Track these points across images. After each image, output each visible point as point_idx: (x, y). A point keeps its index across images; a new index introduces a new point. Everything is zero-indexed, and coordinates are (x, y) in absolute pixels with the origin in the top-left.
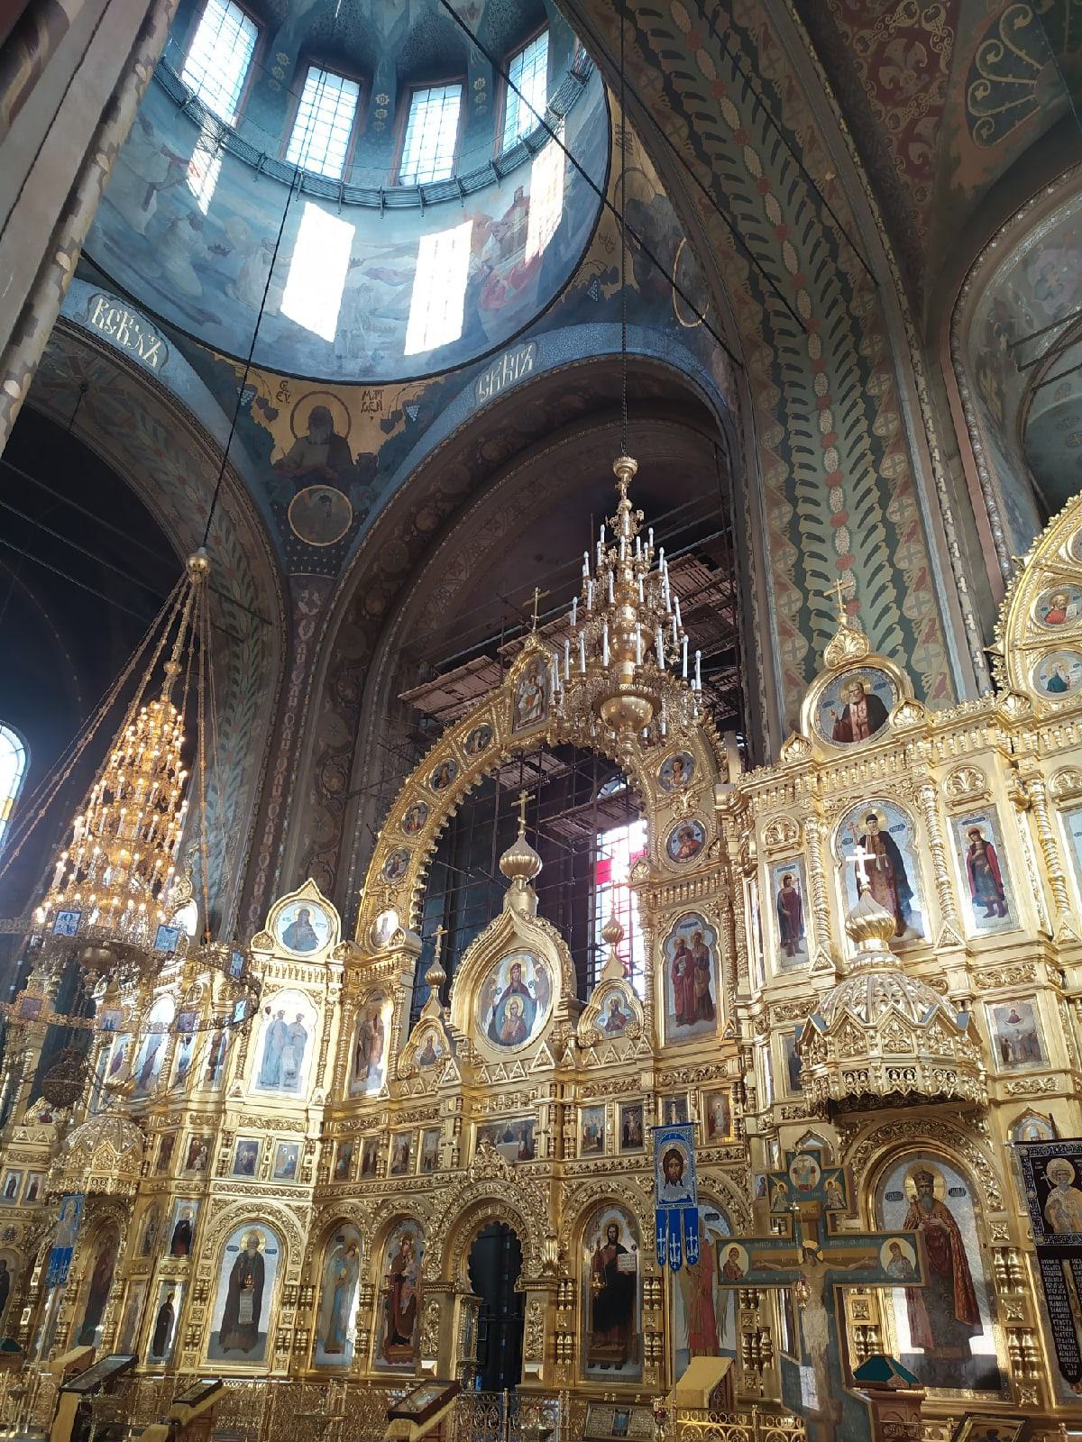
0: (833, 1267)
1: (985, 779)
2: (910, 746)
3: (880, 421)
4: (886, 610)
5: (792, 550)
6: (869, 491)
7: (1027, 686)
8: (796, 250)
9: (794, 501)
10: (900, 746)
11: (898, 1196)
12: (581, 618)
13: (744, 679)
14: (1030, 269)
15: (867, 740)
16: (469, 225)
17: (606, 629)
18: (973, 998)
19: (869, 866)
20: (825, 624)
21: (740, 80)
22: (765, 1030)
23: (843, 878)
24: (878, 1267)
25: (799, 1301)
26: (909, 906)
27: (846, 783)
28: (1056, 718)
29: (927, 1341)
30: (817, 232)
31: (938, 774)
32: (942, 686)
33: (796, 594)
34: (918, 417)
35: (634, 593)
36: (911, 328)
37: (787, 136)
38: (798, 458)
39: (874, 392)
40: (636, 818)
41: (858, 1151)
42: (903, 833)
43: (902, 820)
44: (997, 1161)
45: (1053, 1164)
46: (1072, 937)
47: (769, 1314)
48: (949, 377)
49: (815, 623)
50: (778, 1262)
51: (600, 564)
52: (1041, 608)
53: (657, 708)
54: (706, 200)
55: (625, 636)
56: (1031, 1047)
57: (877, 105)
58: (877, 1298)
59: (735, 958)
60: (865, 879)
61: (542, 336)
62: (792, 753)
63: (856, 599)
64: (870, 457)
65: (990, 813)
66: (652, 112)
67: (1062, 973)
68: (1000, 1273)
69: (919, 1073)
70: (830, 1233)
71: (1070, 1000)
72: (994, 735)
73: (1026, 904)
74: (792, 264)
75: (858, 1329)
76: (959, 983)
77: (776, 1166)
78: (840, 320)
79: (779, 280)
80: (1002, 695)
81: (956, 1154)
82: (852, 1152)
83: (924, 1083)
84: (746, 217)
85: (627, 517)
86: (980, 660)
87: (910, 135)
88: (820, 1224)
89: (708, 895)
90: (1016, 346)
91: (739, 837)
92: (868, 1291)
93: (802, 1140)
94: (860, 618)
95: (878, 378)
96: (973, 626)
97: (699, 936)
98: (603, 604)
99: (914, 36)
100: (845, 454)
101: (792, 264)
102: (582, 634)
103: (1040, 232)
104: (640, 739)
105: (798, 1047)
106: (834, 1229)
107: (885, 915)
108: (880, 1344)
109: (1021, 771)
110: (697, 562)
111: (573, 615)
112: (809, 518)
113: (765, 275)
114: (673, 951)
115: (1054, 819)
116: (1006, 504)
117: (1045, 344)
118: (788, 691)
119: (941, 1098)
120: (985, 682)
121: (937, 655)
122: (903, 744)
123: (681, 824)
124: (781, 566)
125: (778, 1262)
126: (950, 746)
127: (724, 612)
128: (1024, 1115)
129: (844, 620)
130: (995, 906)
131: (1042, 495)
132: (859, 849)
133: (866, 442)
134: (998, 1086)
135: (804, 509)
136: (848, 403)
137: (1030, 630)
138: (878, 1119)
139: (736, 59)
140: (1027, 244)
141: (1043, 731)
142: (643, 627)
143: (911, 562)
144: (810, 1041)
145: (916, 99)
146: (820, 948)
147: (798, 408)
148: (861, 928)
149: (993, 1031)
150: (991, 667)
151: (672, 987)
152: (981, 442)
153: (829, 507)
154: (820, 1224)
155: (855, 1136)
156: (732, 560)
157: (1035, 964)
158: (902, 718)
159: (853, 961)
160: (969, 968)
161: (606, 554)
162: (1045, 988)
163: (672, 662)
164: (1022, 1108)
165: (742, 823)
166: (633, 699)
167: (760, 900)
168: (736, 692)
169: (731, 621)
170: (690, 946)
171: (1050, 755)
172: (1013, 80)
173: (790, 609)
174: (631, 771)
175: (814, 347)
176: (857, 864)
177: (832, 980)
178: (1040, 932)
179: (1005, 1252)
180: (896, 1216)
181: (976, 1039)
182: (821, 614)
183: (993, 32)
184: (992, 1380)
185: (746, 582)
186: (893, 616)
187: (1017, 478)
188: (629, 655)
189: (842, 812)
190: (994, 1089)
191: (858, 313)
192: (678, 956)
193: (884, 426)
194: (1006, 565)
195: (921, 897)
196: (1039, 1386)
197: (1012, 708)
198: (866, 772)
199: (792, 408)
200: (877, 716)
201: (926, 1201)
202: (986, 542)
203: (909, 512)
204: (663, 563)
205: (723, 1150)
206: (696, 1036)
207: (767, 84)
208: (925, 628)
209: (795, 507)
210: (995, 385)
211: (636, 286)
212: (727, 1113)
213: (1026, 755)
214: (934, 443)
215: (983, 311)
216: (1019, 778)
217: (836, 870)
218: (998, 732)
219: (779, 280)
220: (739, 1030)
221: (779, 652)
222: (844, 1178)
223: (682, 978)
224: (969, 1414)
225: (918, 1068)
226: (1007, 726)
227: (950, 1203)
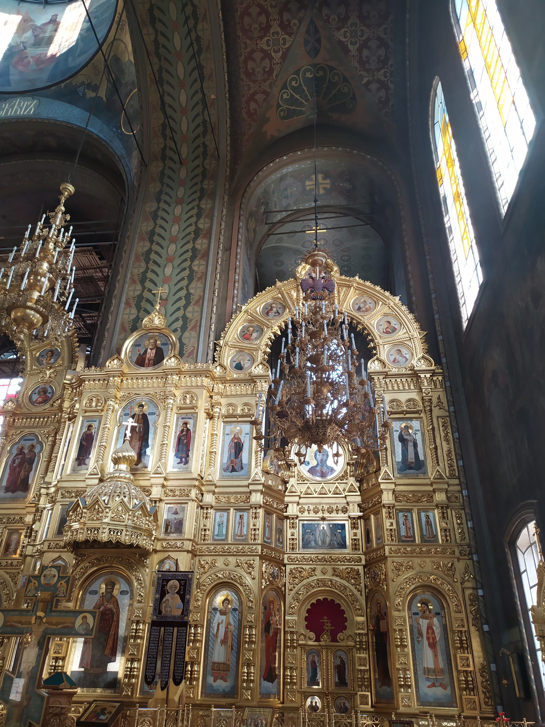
0: (49, 626)
1: (197, 401)
2: (170, 376)
3: (202, 221)
4: (178, 309)
5: (143, 264)
6: (187, 251)
7: (227, 363)
8: (188, 123)
9: (152, 242)
10: (165, 375)
11: (96, 592)
12: (15, 258)
13: (100, 320)
14: (282, 182)
15: (151, 368)
16: (19, 18)
17: (28, 270)
18: (161, 500)
19: (133, 428)
20: (148, 307)
21: (186, 30)
22: (53, 501)
23: (118, 432)
24: (73, 627)
25: (25, 643)
26: (145, 452)
27: (135, 386)
28: (235, 381)
29: (87, 665)
30: (199, 120)
31: (178, 393)
32: (191, 353)
33: (139, 287)
34: (218, 226)
35: (51, 256)
36: (227, 185)
37: (199, 67)
38: (160, 221)
39: (203, 206)
40: (16, 376)
41: (82, 568)
42: (154, 416)
43: (154, 411)
44: (148, 579)
45: (171, 583)
46: (211, 479)
47: (7, 650)
48: (237, 214)
49: (144, 304)
50: (20, 622)
51: (36, 234)
52: (242, 331)
53: (45, 321)
54: (152, 76)
55: (39, 278)
56: (179, 526)
57: (243, 76)
58: (69, 643)
59: (49, 461)
60: (129, 434)
61: (45, 99)
62: (112, 364)
63: (166, 300)
64: (193, 235)
65: (194, 417)
66: (140, 20)
67: (202, 495)
68: (133, 632)
69: (124, 533)
70: (53, 609)
71: (202, 508)
72: (206, 381)
73: (197, 461)
74: (184, 127)
75: (53, 659)
76: (156, 492)
77: (37, 572)
78: (198, 166)
79: (176, 133)
80: (217, 364)
81: (128, 573)
82: (78, 569)
83: (125, 538)
84: (169, 94)
85: (60, 215)
86: (211, 345)
87: (252, 98)
88: (50, 604)
89: (46, 425)
90: (267, 213)
91: (72, 400)
92: (65, 639)
93: (54, 561)
94: (165, 309)
95: (207, 201)
96: (213, 329)
97: (33, 446)
98: (31, 257)
99: (267, 55)
100: (182, 229)
101: (184, 127)
102: (13, 268)
103: (290, 169)
104: (31, 334)
105: (68, 513)
106: (56, 607)
107: (133, 454)
108: (63, 667)
109: (213, 401)
110: (94, 253)
111: (12, 256)
112: (157, 253)
113: (170, 128)
114: (15, 452)
115: (220, 425)
116: (243, 280)
117: (279, 217)
118: (120, 334)
119: (131, 546)
120: (210, 357)
121: (195, 338)
122: (167, 375)
123: (42, 385)
124: (136, 271)
125: (20, 622)
126: (187, 381)
127: (101, 284)
128: (166, 558)
129: (158, 308)
130: (184, 459)
131: (258, 282)
132: (131, 420)
133: (193, 228)
134: (159, 544)
135: (155, 247)
136: (190, 206)
137: (235, 339)
138: (97, 553)
139: (187, 18)
140: (284, 171)
141: (227, 385)
142: (51, 276)
143: (196, 291)
144: (75, 510)
145: (260, 83)
146: (96, 464)
147: (167, 198)
148: (119, 458)
149: (165, 517)
150: (215, 350)
151: (8, 471)
152: (241, 248)
153: (167, 251)
154: (50, 604)
155: (83, 561)
156: (113, 259)
157: (192, 489)
158: (170, 362)
159: (110, 474)
160: (163, 486)
161: (41, 230)
162: (193, 500)
163: (62, 300)
164: (166, 554)
165: (76, 393)
166: (33, 312)
167: (72, 434)
168: (94, 325)
169: (103, 289)
170: (26, 451)
171: (227, 396)
172: (299, 98)
173: (134, 293)
174: (21, 349)
175: (183, 173)
176: (127, 426)
177: (97, 481)
178: (199, 475)
179: (138, 623)
180: (91, 602)
181: (156, 519)
182: (148, 301)
183: (297, 72)
184: (113, 683)
185: (116, 273)
186: (180, 314)
187: (250, 271)
188: (38, 288)
189: (129, 400)
190: (157, 545)
191: (207, 167)
192: (17, 455)
193: (203, 224)
194: (234, 307)
195: (152, 448)
196: (133, 686)
197: (218, 371)
198: (145, 383)
199: (164, 197)
200: (159, 358)
201: (109, 596)
202: (230, 294)
203: (202, 268)
204: (73, 247)
205: (10, 562)
206: (14, 500)
207: (198, 38)
208: (193, 323)
209: (152, 245)
210: (254, 226)
211: (104, 99)
212: (18, 542)
213: (217, 394)
214: (221, 241)
215: (259, 191)
216: (211, 404)
217: (116, 427)
218: (209, 380)
219: (176, 133)
220: (39, 500)
221: (123, 313)
222: (70, 582)
223: (16, 467)
224: (95, 701)
225: (124, 531)
226: (213, 379)
227: (119, 597)
